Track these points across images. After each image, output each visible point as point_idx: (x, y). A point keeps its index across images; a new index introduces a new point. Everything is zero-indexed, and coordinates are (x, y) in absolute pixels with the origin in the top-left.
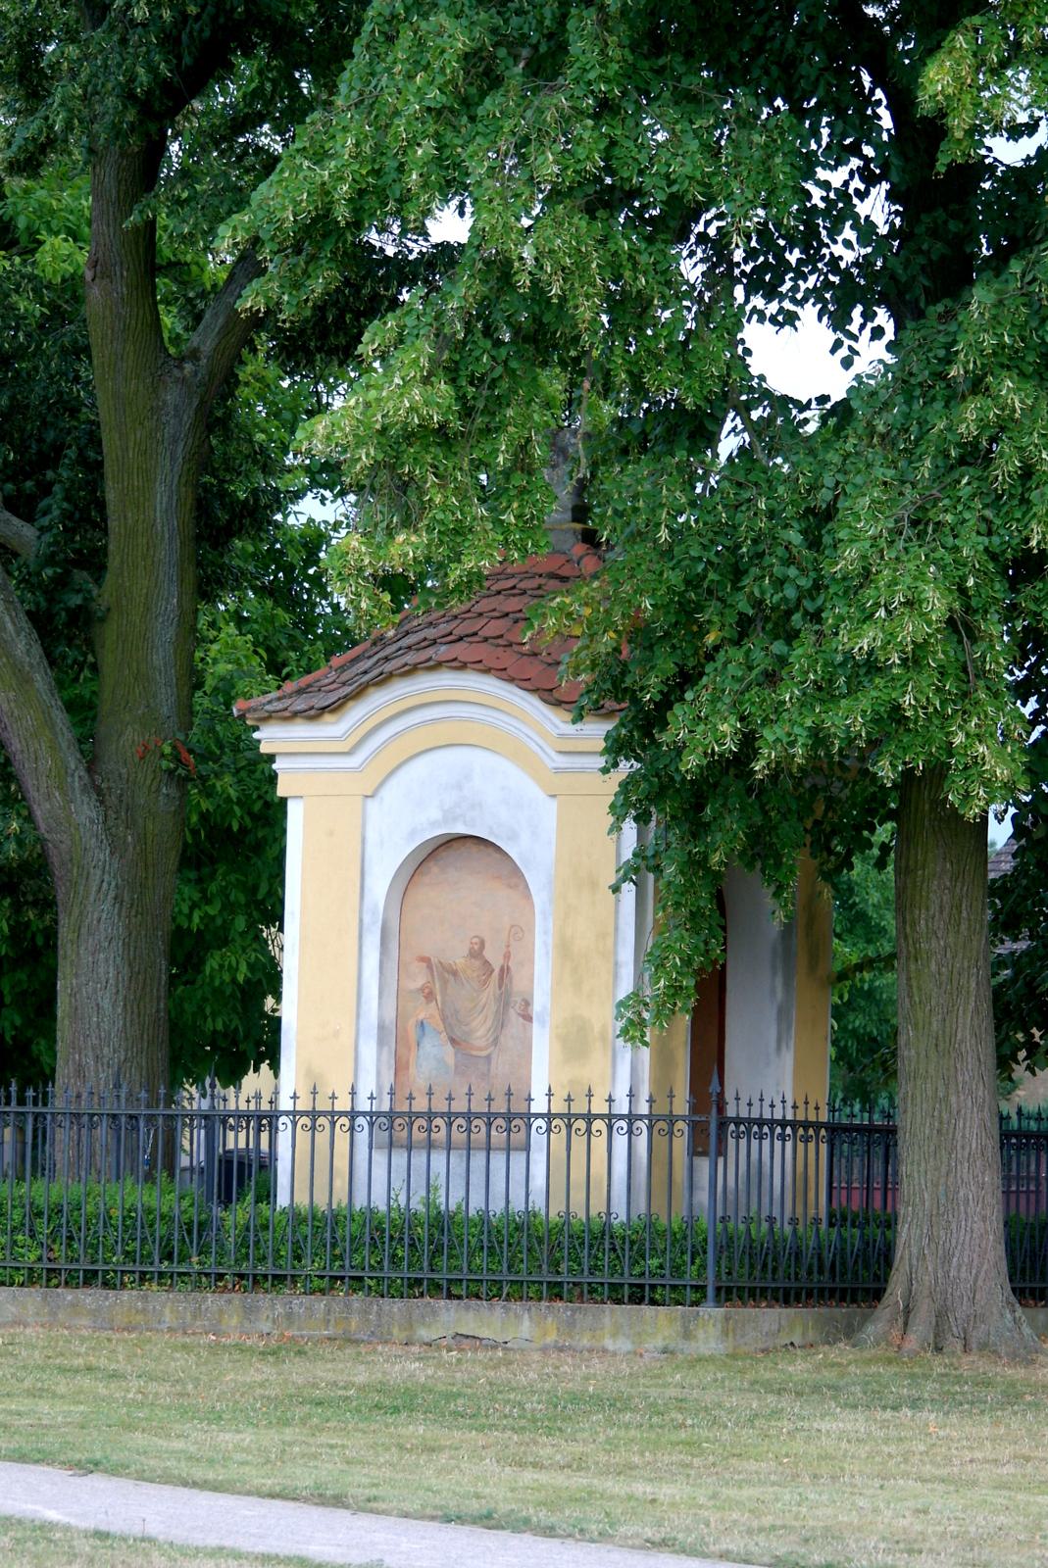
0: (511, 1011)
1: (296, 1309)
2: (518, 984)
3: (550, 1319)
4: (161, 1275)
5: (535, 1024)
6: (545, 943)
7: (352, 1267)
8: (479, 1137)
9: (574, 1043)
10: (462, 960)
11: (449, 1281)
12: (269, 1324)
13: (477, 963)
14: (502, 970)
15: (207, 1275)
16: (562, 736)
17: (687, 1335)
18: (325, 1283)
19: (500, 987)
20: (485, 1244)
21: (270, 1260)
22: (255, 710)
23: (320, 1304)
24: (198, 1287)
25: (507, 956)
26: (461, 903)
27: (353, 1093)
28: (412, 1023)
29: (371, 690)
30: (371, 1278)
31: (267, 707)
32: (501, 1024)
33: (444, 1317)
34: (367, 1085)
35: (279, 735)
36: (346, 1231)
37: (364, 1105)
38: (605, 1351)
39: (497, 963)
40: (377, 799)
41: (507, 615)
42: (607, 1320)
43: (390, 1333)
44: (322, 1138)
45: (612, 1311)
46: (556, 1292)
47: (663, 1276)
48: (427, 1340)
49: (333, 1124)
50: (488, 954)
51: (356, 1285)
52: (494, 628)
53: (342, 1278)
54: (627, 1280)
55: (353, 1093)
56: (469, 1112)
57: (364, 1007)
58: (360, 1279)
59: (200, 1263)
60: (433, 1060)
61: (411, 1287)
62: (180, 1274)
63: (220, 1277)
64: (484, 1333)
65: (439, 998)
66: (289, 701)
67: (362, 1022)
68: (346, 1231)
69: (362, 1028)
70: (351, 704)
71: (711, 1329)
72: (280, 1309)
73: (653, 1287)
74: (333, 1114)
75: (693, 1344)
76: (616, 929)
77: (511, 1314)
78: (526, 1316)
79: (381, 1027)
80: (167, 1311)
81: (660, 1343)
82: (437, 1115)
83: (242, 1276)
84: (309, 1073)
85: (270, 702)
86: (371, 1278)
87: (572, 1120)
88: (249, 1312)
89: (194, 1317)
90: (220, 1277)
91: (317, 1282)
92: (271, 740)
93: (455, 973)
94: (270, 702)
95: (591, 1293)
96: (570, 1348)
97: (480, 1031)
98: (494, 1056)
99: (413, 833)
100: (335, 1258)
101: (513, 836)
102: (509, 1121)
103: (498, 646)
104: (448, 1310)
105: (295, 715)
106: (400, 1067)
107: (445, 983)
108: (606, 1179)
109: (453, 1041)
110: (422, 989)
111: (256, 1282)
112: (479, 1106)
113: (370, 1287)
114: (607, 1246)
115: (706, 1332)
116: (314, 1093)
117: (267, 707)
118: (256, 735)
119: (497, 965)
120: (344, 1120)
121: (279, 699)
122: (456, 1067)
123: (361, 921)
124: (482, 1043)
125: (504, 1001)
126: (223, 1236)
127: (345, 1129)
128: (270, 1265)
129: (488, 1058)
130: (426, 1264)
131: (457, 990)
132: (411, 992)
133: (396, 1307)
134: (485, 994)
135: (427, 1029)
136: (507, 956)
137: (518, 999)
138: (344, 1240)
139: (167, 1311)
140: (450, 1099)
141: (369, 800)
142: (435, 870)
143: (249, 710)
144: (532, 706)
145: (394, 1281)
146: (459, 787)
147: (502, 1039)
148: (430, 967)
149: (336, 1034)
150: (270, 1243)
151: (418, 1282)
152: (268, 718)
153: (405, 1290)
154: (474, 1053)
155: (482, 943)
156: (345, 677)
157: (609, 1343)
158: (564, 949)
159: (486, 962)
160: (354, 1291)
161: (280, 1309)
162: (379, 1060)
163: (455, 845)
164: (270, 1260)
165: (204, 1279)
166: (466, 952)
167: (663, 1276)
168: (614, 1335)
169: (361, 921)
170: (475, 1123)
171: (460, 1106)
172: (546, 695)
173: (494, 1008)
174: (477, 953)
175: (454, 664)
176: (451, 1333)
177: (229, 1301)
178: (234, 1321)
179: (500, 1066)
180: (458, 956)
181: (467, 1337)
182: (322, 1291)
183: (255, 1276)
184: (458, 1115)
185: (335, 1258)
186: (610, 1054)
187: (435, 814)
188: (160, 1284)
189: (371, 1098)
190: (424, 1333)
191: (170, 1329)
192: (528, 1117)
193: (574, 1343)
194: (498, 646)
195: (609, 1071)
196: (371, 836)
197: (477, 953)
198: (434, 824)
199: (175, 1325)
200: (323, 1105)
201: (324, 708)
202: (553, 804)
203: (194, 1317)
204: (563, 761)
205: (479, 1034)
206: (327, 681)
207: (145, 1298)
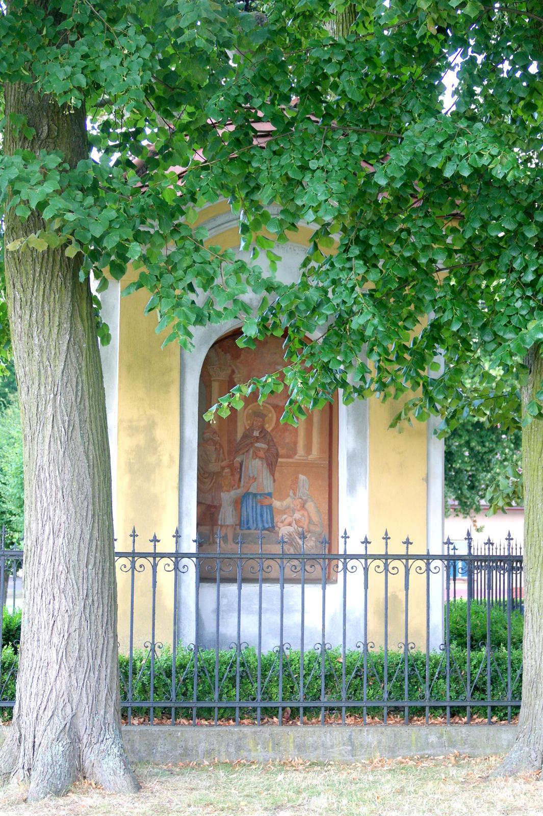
116: (134, 535)
192: (338, 557)
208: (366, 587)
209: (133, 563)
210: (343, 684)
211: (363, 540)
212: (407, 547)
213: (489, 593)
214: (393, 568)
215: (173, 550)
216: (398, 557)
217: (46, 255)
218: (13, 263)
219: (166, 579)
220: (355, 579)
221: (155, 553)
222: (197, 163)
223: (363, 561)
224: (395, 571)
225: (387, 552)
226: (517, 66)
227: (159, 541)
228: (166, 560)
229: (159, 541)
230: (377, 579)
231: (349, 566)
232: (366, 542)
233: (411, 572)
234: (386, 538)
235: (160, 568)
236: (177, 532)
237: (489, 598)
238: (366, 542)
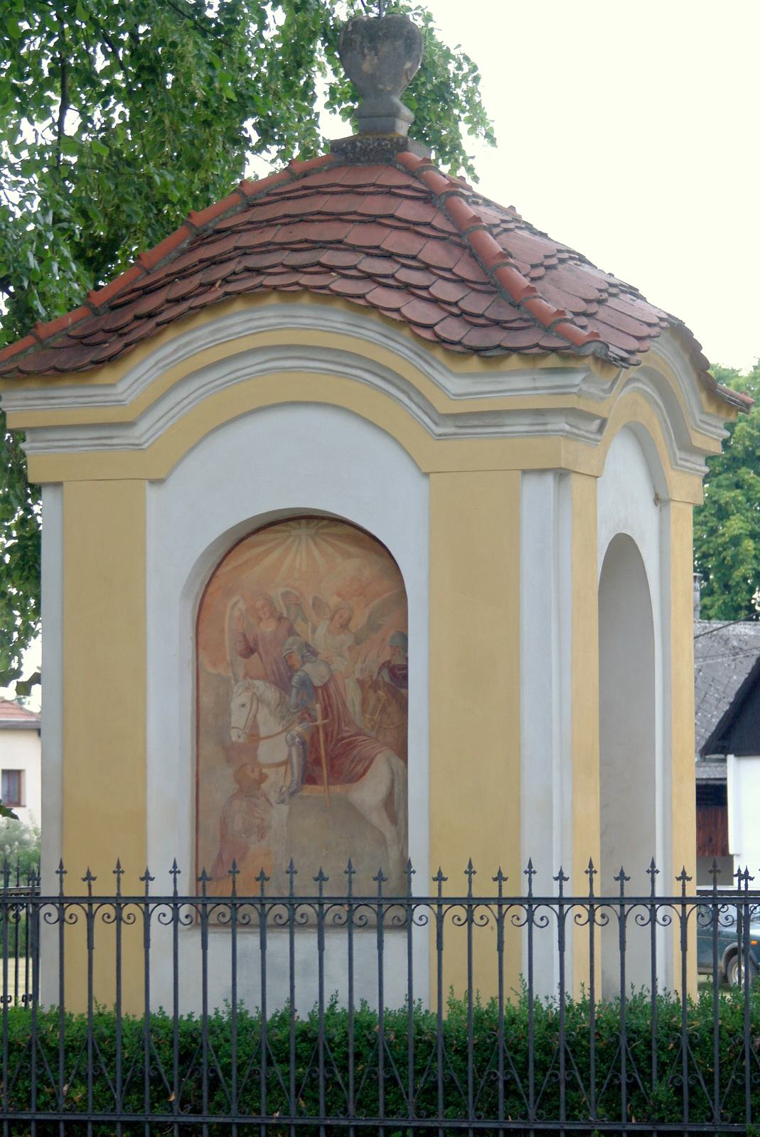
200: (132, 888)
208: (90, 947)
210: (232, 1087)
211: (85, 876)
215: (112, 893)
217: (120, 332)
220: (422, 935)
222: (29, 212)
223: (495, 908)
224: (544, 923)
225: (175, 892)
226: (141, 156)
227: (445, 879)
228: (578, 909)
229: (628, 879)
230: (455, 935)
231: (537, 918)
232: (380, 878)
233: (628, 924)
234: (470, 872)
238: (561, 878)
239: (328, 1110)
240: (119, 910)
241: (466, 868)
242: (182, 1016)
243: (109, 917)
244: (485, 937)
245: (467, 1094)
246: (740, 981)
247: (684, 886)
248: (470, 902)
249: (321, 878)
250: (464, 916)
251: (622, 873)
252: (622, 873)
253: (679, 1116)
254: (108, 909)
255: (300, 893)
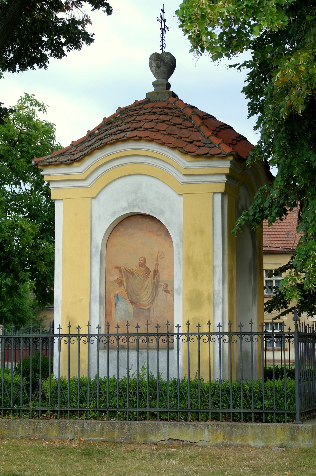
0: (159, 289)
1: (86, 427)
2: (163, 276)
3: (219, 432)
4: (14, 411)
5: (175, 295)
6: (179, 258)
7: (110, 406)
8: (153, 344)
9: (195, 301)
10: (135, 268)
11: (160, 412)
12: (73, 435)
13: (143, 269)
14: (155, 271)
15: (36, 411)
16: (187, 168)
17: (293, 438)
18: (97, 414)
19: (154, 278)
20: (178, 394)
21: (69, 404)
22: (42, 162)
23: (98, 425)
24: (32, 417)
25: (157, 265)
26: (139, 244)
27: (89, 326)
28: (112, 295)
29: (96, 151)
30: (120, 411)
31: (48, 161)
32: (155, 294)
33: (163, 430)
34: (218, 320)
35: (53, 172)
36: (107, 388)
37: (95, 331)
38: (249, 446)
39: (152, 268)
40: (97, 199)
41: (152, 121)
42: (250, 432)
43: (135, 438)
44: (74, 346)
45: (252, 427)
46: (227, 417)
47: (272, 409)
48: (154, 442)
49: (79, 340)
50: (148, 264)
51: (111, 414)
52: (147, 125)
53: (105, 412)
54: (253, 411)
55: (89, 326)
56: (69, 334)
57: (93, 289)
58: (115, 412)
59: (34, 405)
60: (123, 311)
61: (140, 415)
62: (23, 411)
63: (44, 412)
64: (184, 438)
65: (125, 284)
66: (57, 158)
67: (92, 295)
68: (107, 388)
69: (92, 298)
70: (86, 158)
71: (306, 435)
72: (78, 427)
73: (266, 414)
74: (79, 336)
75: (297, 443)
76: (213, 251)
77: (199, 429)
78: (206, 430)
79: (101, 297)
80: (20, 429)
81: (279, 442)
82: (151, 334)
83: (54, 411)
84: (68, 317)
85: (48, 159)
86: (120, 411)
87: (194, 335)
88: (62, 429)
89: (34, 432)
90: (44, 412)
91: (93, 414)
92: (49, 175)
93: (132, 273)
94: (48, 159)
95: (235, 418)
96: (230, 445)
97: (145, 298)
98: (152, 309)
99: (114, 213)
100: (101, 402)
101: (162, 213)
102: (165, 337)
103: (153, 131)
104: (165, 427)
105: (62, 163)
106: (107, 314)
107: (127, 278)
108: (212, 363)
109: (132, 303)
110: (117, 281)
111: (61, 414)
112: (152, 330)
113: (119, 415)
114: (242, 395)
115: (303, 437)
116: (69, 326)
117: (48, 161)
118: (42, 173)
119: (152, 268)
120: (84, 338)
121: (52, 158)
122: (134, 313)
123: (91, 251)
124: (145, 303)
125: (156, 284)
126: (33, 390)
127: (104, 342)
128: (68, 405)
129: (149, 310)
130: (148, 405)
131: (134, 281)
132: (112, 282)
133: (137, 425)
134: (147, 282)
135: (119, 298)
136: (157, 265)
137: (163, 284)
138: (105, 393)
139: (20, 429)
140: (118, 327)
141: (93, 200)
142: (122, 229)
143: (40, 162)
144: (174, 156)
145: (132, 413)
146: (135, 192)
147: (155, 301)
148: (120, 271)
149: (80, 301)
150: (68, 396)
151: (143, 413)
152: (46, 166)
153: (138, 417)
154: (143, 307)
155: (145, 260)
156: (80, 148)
157: (251, 443)
158: (188, 261)
159: (147, 268)
160: (111, 417)
161: (78, 427)
162: (100, 311)
163: (131, 218)
164: (69, 404)
165: (35, 413)
166: (138, 264)
167: (272, 409)
168: (254, 439)
169: (91, 251)
170: (150, 338)
171: (142, 330)
172: (181, 149)
173: (151, 288)
174: (143, 264)
175: (136, 138)
176: (167, 438)
177: (52, 424)
178: (54, 434)
179: (155, 313)
180: (133, 265)
181: (175, 440)
182: (95, 418)
183: (61, 411)
184: (162, 334)
185: (101, 402)
186: (212, 306)
187: (124, 204)
188: (14, 416)
189: (219, 326)
190: (152, 438)
191: (22, 438)
192: (173, 334)
193: (232, 443)
194: (153, 131)
195: (212, 313)
196: (95, 215)
197: (143, 264)
198: (124, 209)
199: (24, 435)
200: (74, 331)
201: (74, 160)
202: (182, 199)
203: (34, 432)
204: (186, 179)
205: (144, 299)
206: (72, 150)
207: (9, 423)
209: (188, 338)
212: (178, 329)
213: (305, 353)
214: (192, 339)
215: (186, 332)
216: (194, 334)
218: (221, 180)
219: (84, 348)
221: (178, 333)
224: (113, 342)
225: (188, 331)
231: (71, 341)
232: (158, 327)
235: (181, 340)
236: (89, 323)
237: (305, 358)
239: (244, 408)
240: (148, 338)
241: (126, 323)
242: (191, 379)
243: (85, 341)
244: (194, 346)
245: (230, 400)
246: (8, 363)
247: (199, 329)
248: (209, 334)
249: (138, 327)
250: (87, 340)
251: (199, 324)
252: (199, 324)
253: (259, 407)
254: (205, 337)
255: (92, 333)
